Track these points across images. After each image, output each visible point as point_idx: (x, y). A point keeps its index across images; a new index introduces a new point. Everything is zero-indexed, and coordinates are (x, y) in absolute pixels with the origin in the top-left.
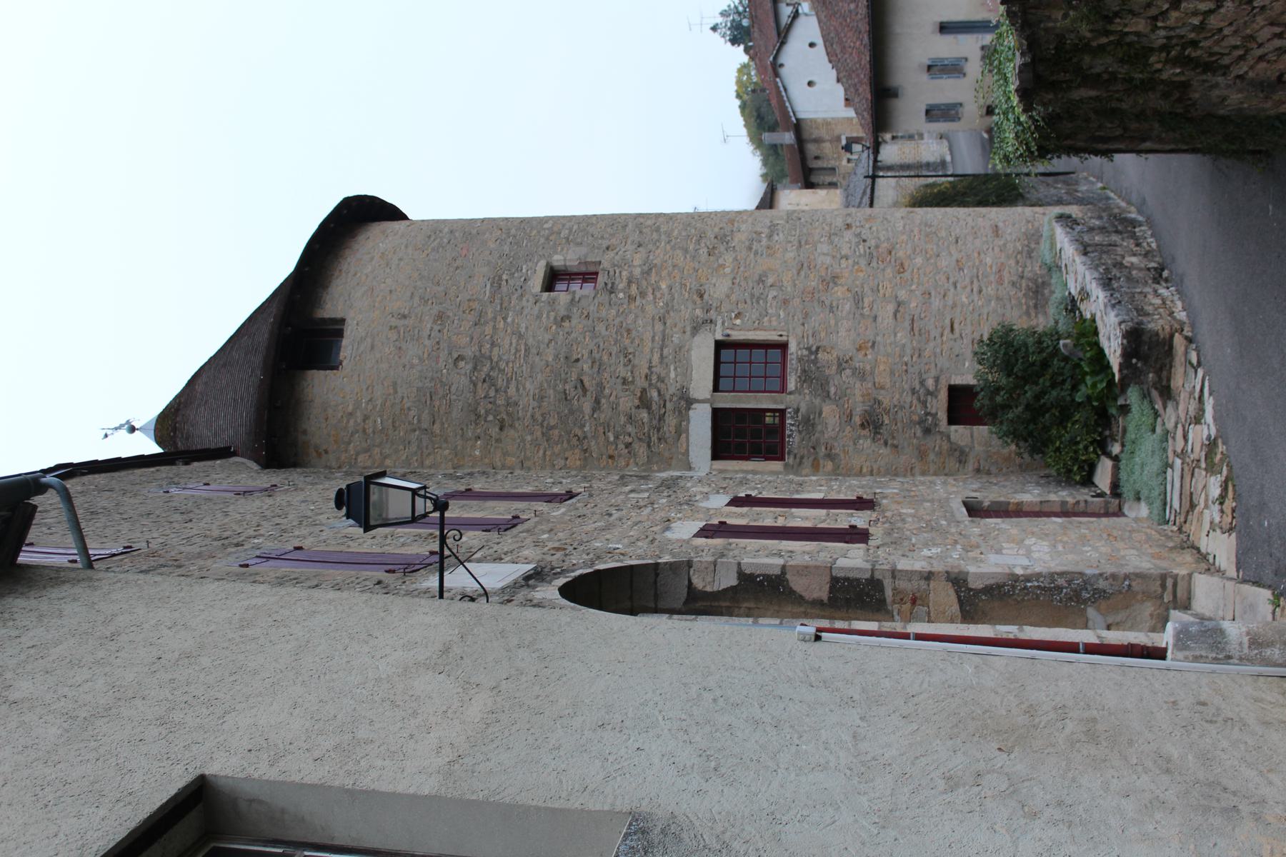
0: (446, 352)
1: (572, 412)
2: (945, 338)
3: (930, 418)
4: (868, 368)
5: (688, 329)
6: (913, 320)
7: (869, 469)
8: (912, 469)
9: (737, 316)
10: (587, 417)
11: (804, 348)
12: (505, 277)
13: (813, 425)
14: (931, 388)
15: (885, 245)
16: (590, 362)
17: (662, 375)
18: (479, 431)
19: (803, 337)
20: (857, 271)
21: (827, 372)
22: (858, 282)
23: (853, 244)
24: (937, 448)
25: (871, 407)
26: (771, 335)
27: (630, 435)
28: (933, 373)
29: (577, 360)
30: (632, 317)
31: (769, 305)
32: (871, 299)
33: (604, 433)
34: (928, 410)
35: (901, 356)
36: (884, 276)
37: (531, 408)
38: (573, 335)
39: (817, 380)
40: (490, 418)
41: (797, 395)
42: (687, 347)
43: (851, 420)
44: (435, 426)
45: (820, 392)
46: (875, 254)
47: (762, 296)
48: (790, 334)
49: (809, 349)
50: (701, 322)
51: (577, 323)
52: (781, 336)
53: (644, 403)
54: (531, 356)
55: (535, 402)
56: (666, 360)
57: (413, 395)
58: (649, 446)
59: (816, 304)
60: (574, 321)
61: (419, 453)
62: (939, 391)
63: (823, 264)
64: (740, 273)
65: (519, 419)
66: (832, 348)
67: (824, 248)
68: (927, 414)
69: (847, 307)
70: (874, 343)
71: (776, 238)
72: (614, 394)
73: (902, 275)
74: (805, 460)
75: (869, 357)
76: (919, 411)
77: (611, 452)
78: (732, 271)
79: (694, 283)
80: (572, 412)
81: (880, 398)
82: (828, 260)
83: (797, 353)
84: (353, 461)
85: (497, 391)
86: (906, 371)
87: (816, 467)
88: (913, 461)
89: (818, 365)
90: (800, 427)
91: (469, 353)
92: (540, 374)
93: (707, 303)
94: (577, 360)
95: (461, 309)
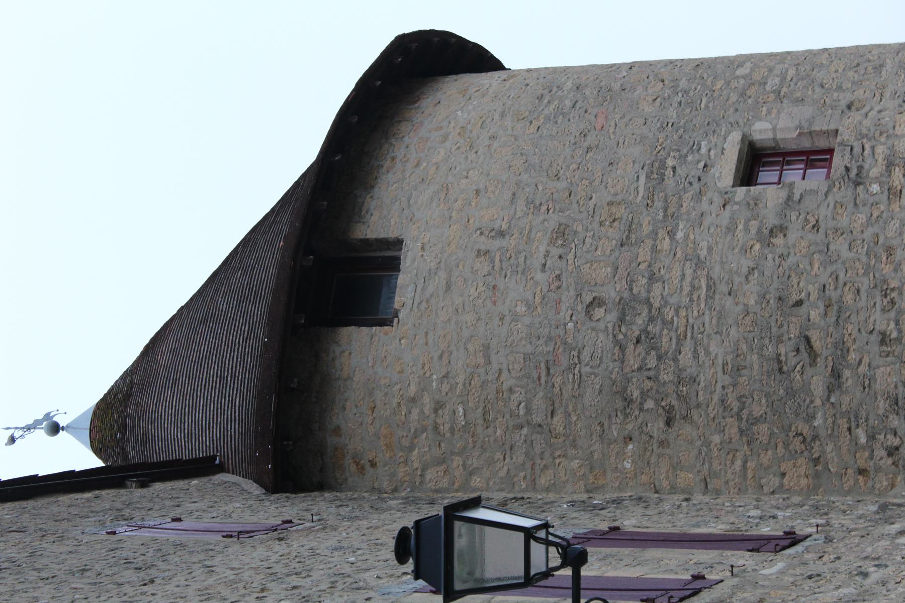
0: (572, 293)
1: (791, 393)
10: (818, 402)
16: (821, 305)
18: (630, 427)
29: (799, 303)
33: (849, 429)
37: (719, 385)
38: (792, 260)
40: (650, 404)
44: (555, 419)
60: (793, 235)
61: (528, 465)
65: (698, 406)
72: (866, 360)
80: (791, 393)
85: (659, 358)
91: (611, 293)
94: (799, 303)
95: (597, 219)
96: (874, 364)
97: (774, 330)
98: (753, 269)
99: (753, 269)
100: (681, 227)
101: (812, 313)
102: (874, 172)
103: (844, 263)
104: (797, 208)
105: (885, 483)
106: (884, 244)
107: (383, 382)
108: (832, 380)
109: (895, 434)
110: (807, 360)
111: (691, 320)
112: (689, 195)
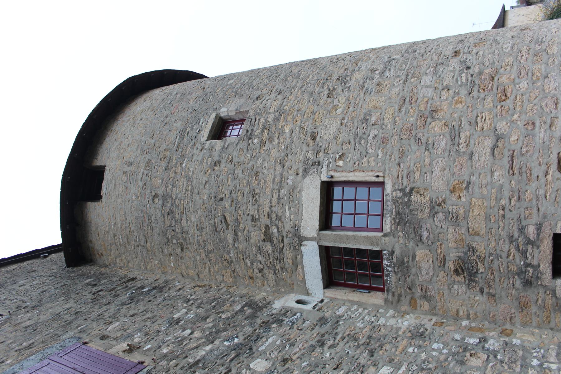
0: (149, 191)
1: (221, 241)
2: (549, 177)
3: (531, 270)
4: (462, 212)
5: (301, 171)
6: (512, 156)
7: (465, 313)
8: (511, 318)
9: (341, 158)
10: (231, 246)
11: (399, 190)
13: (407, 268)
14: (532, 237)
15: (489, 70)
16: (229, 200)
17: (280, 214)
18: (170, 249)
19: (398, 177)
20: (457, 102)
21: (420, 216)
22: (456, 115)
23: (457, 72)
24: (540, 301)
25: (465, 253)
26: (369, 176)
27: (261, 263)
28: (535, 219)
29: (222, 199)
30: (261, 159)
31: (369, 144)
32: (468, 133)
33: (243, 259)
34: (528, 262)
35: (498, 199)
36: (483, 106)
37: (196, 235)
38: (221, 177)
39: (410, 223)
40: (175, 241)
41: (392, 237)
42: (298, 189)
43: (444, 265)
44: (148, 244)
45: (413, 235)
46: (477, 82)
47: (365, 136)
48: (386, 175)
49: (402, 190)
50: (311, 164)
51: (224, 166)
52: (378, 176)
53: (268, 238)
54: (194, 195)
55: (198, 232)
56: (282, 201)
57: (134, 222)
58: (275, 272)
59: (412, 141)
60: (223, 165)
61: (143, 261)
62: (542, 241)
63: (424, 97)
64: (349, 113)
65: (190, 243)
66: (425, 189)
67: (427, 80)
68: (527, 265)
69: (443, 144)
70: (469, 184)
71: (387, 73)
72: (247, 228)
73: (503, 103)
74: (403, 298)
75: (463, 199)
76: (518, 260)
77: (250, 274)
78: (343, 111)
79: (310, 126)
80: (221, 241)
81: (474, 245)
82: (430, 92)
83: (392, 194)
84: (115, 262)
85: (176, 222)
86: (503, 216)
87: (413, 304)
88: (513, 311)
89: (411, 208)
90: (396, 268)
91: (161, 192)
92: (199, 210)
93: (318, 144)
94: (222, 199)
95: (160, 157)
96: (250, 230)
97: (213, 212)
98: (207, 182)
99: (207, 182)
100: (185, 161)
101: (226, 204)
102: (257, 132)
103: (239, 180)
104: (225, 151)
105: (260, 284)
106: (255, 170)
107: (100, 224)
108: (235, 237)
109: (261, 263)
110: (225, 227)
111: (185, 206)
112: (190, 145)
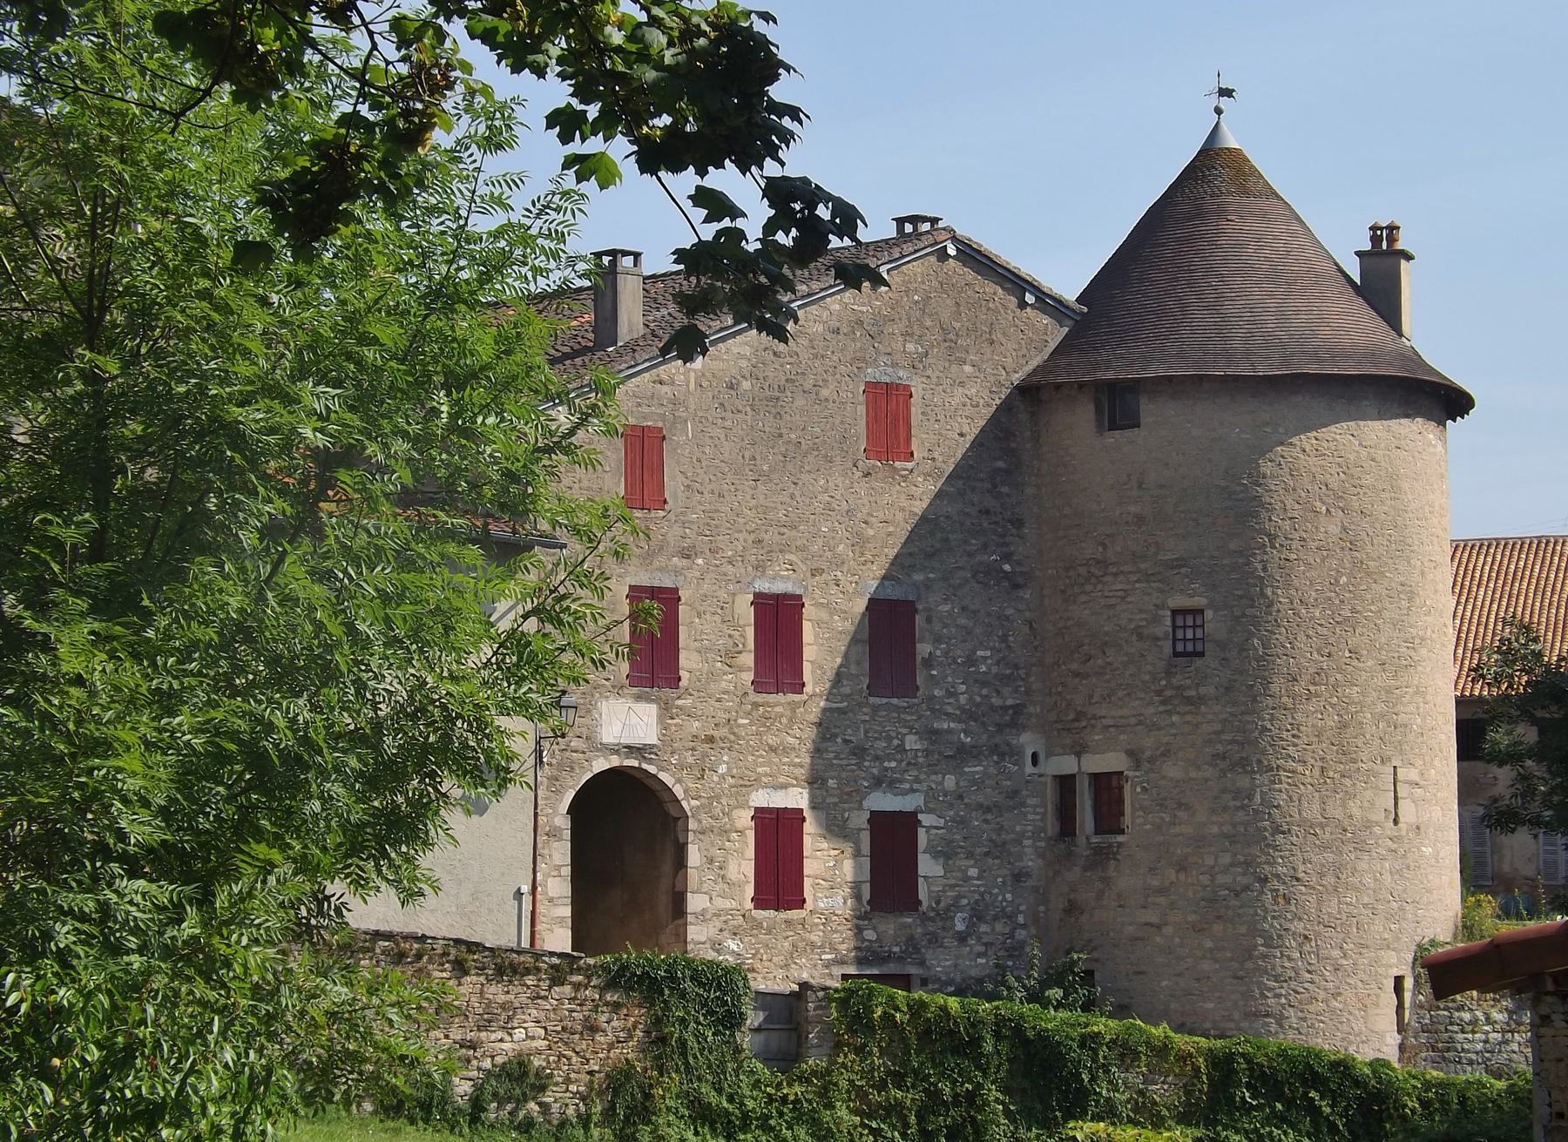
9: (1144, 788)
12: (1183, 570)
